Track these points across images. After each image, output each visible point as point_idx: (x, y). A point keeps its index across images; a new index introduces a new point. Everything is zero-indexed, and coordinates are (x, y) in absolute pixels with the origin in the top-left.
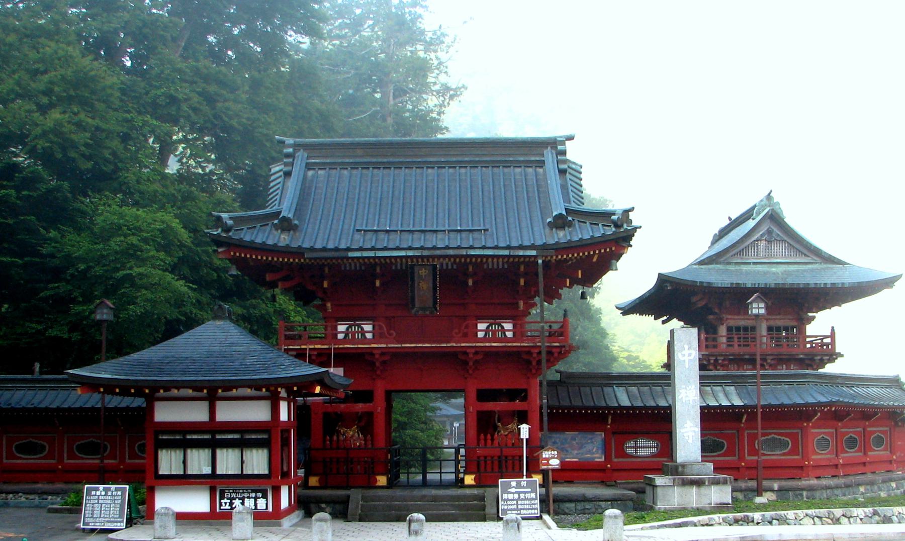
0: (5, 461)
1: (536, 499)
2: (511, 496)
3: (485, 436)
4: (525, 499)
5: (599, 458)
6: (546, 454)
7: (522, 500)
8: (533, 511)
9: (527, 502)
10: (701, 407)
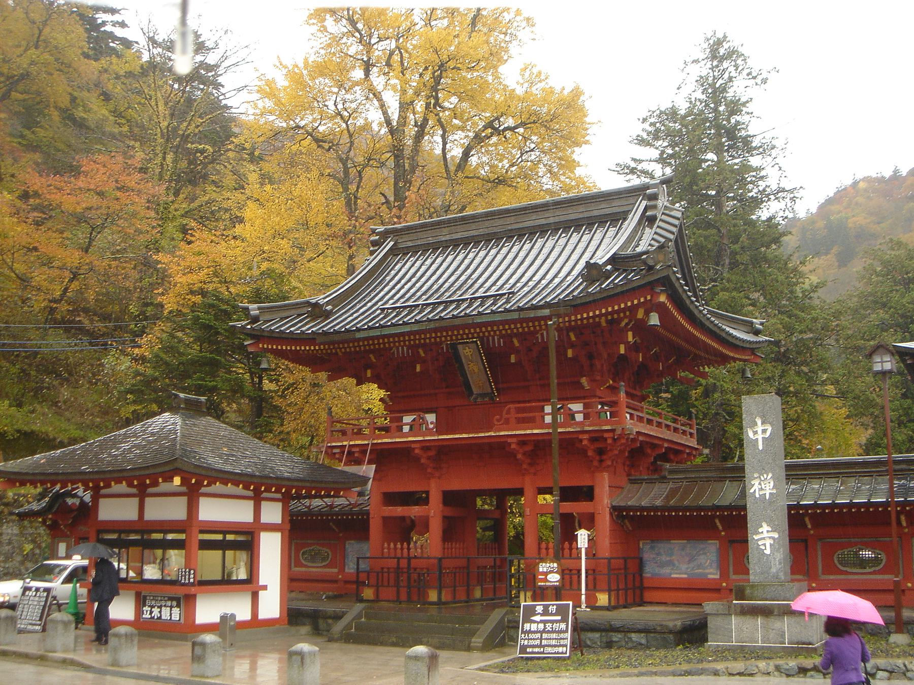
0: (571, 603)
1: (566, 631)
2: (534, 627)
3: (402, 545)
4: (553, 632)
5: (713, 574)
6: (543, 567)
7: (549, 632)
8: (560, 649)
9: (554, 636)
10: (790, 507)
